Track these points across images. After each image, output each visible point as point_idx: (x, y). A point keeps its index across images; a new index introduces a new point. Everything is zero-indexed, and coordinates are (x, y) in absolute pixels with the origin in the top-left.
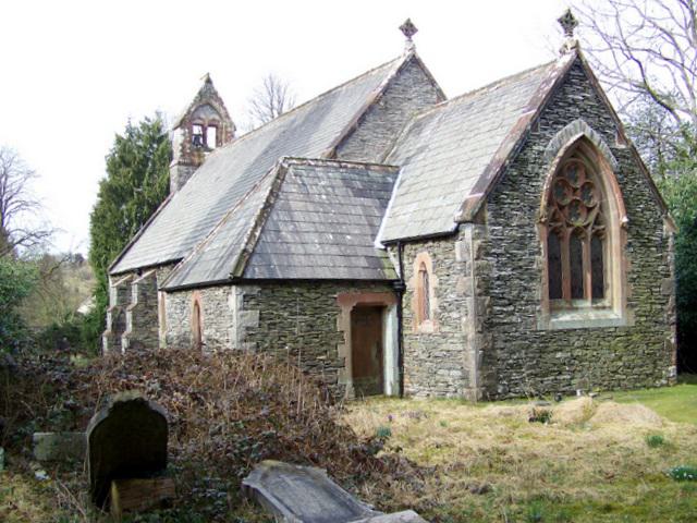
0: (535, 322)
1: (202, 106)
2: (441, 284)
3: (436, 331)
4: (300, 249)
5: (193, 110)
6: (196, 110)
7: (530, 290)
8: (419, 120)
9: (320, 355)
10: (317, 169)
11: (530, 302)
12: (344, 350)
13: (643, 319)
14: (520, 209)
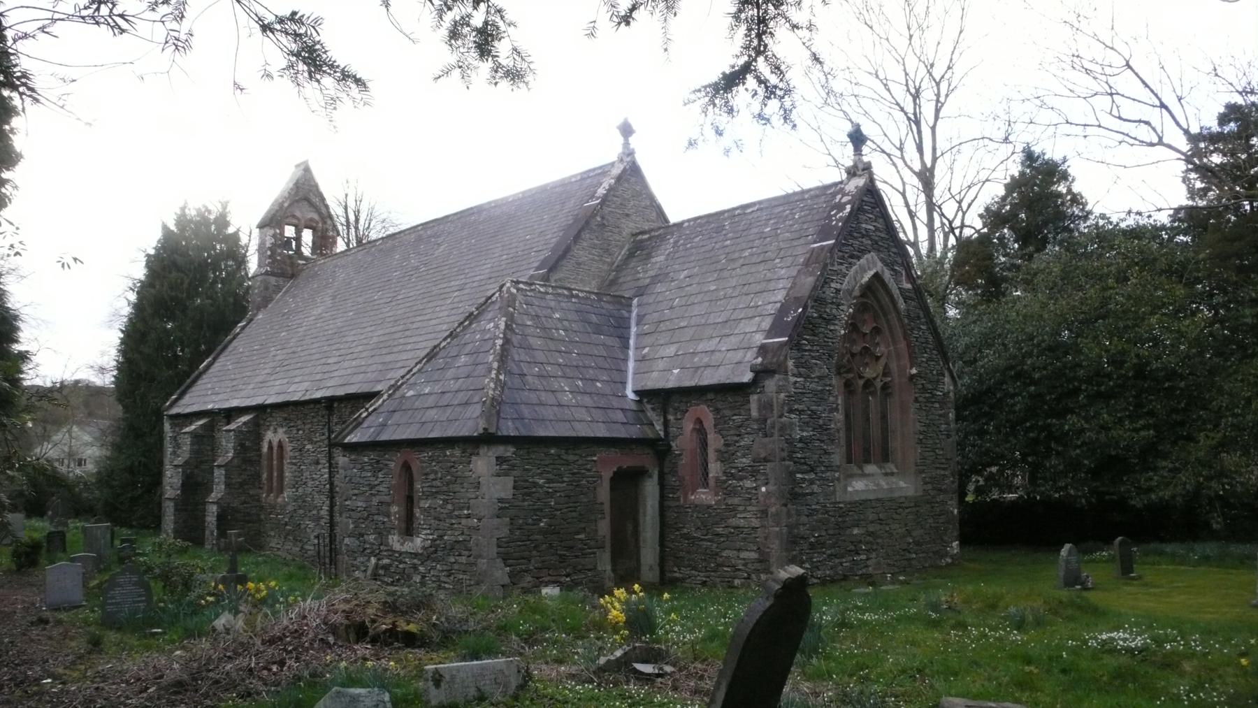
0: (834, 492)
1: (297, 201)
2: (727, 445)
3: (718, 502)
4: (550, 399)
5: (286, 205)
6: (290, 205)
7: (829, 454)
8: (642, 241)
9: (578, 533)
10: (548, 297)
11: (829, 468)
12: (604, 527)
13: (930, 486)
14: (819, 358)
